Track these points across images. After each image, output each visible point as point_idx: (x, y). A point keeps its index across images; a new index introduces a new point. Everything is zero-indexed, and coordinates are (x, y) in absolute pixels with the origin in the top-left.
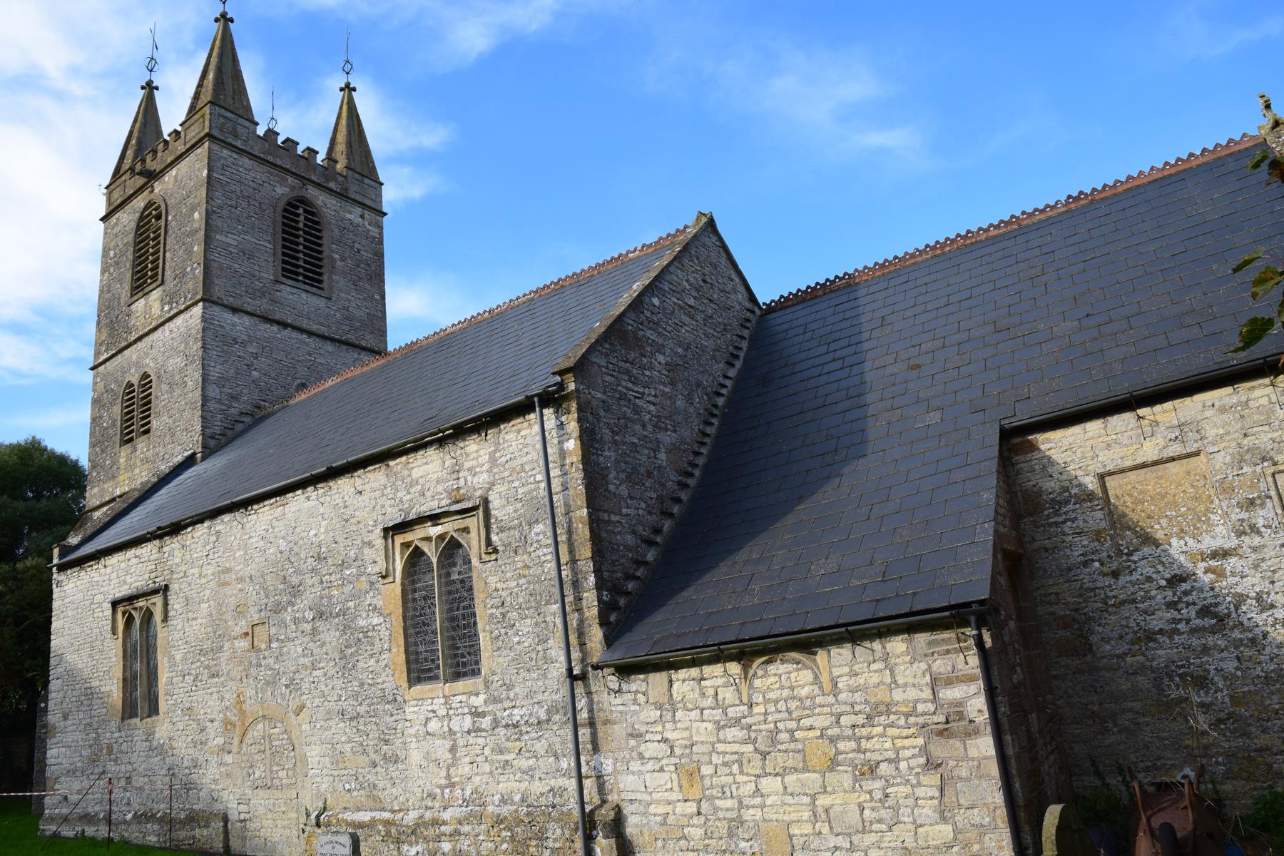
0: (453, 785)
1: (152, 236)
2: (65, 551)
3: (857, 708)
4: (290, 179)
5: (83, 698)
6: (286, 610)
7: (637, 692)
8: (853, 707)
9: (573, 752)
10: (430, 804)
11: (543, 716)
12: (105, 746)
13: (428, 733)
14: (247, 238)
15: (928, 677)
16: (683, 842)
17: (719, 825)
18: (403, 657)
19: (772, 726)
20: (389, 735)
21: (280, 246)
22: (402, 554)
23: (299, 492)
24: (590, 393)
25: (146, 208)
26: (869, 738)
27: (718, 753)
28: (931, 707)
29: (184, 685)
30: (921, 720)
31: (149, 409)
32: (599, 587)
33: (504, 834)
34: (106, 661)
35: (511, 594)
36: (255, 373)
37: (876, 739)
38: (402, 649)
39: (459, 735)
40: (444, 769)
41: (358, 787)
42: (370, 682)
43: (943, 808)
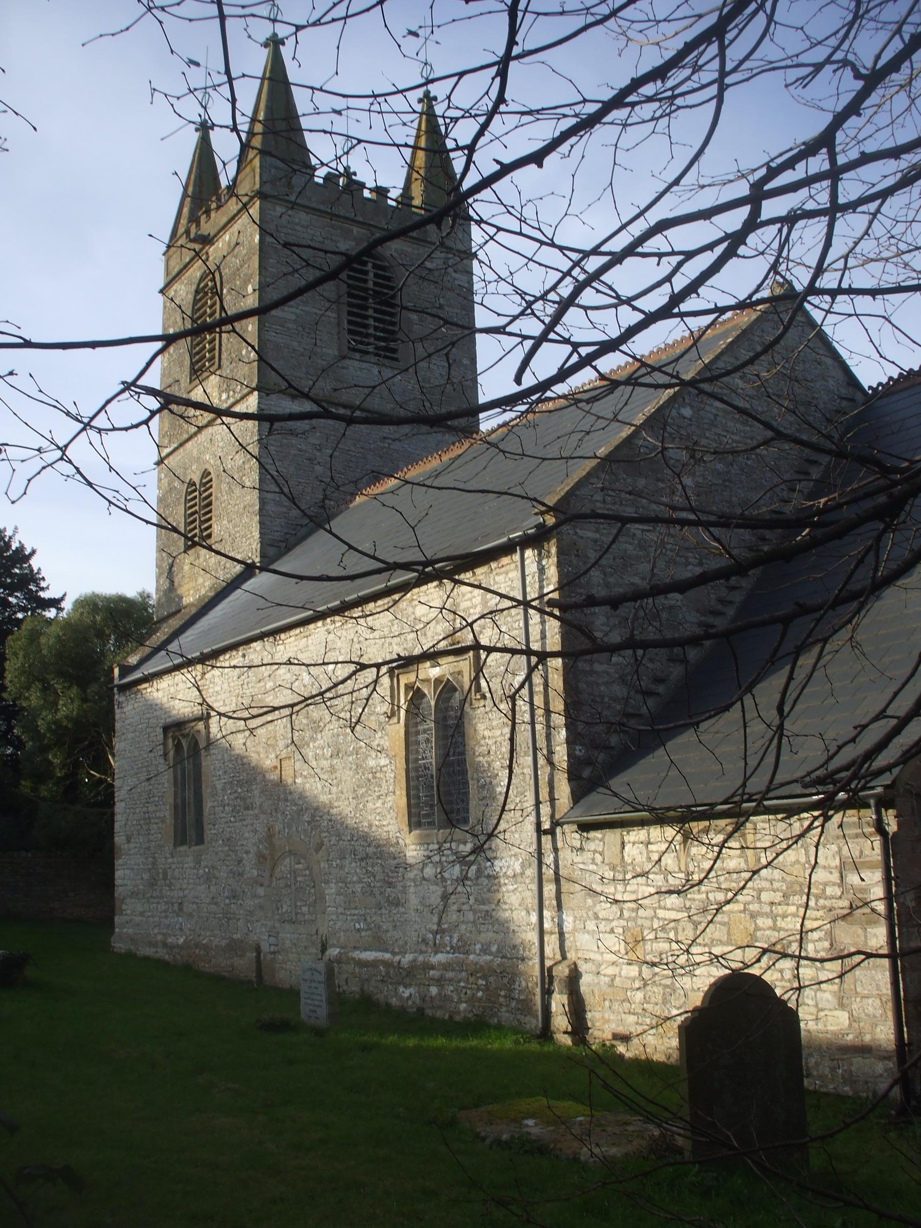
0: (443, 931)
1: (208, 311)
2: (126, 670)
3: (776, 885)
4: (355, 230)
5: (142, 822)
6: (308, 746)
7: (595, 851)
8: (772, 884)
9: (536, 907)
10: (424, 948)
11: (518, 869)
12: (161, 871)
13: (424, 879)
14: (307, 309)
15: (837, 862)
16: (626, 1005)
17: (656, 990)
18: (405, 799)
19: (704, 896)
20: (393, 877)
21: (346, 314)
22: (406, 694)
23: (320, 624)
24: (576, 533)
25: (202, 279)
26: (784, 916)
27: (658, 918)
28: (838, 892)
29: (224, 815)
30: (828, 903)
31: (210, 511)
32: (569, 742)
33: (481, 982)
34: (160, 787)
35: (496, 743)
36: (317, 468)
37: (789, 918)
38: (404, 793)
39: (449, 882)
40: (436, 915)
41: (366, 927)
42: (377, 823)
43: (842, 994)
